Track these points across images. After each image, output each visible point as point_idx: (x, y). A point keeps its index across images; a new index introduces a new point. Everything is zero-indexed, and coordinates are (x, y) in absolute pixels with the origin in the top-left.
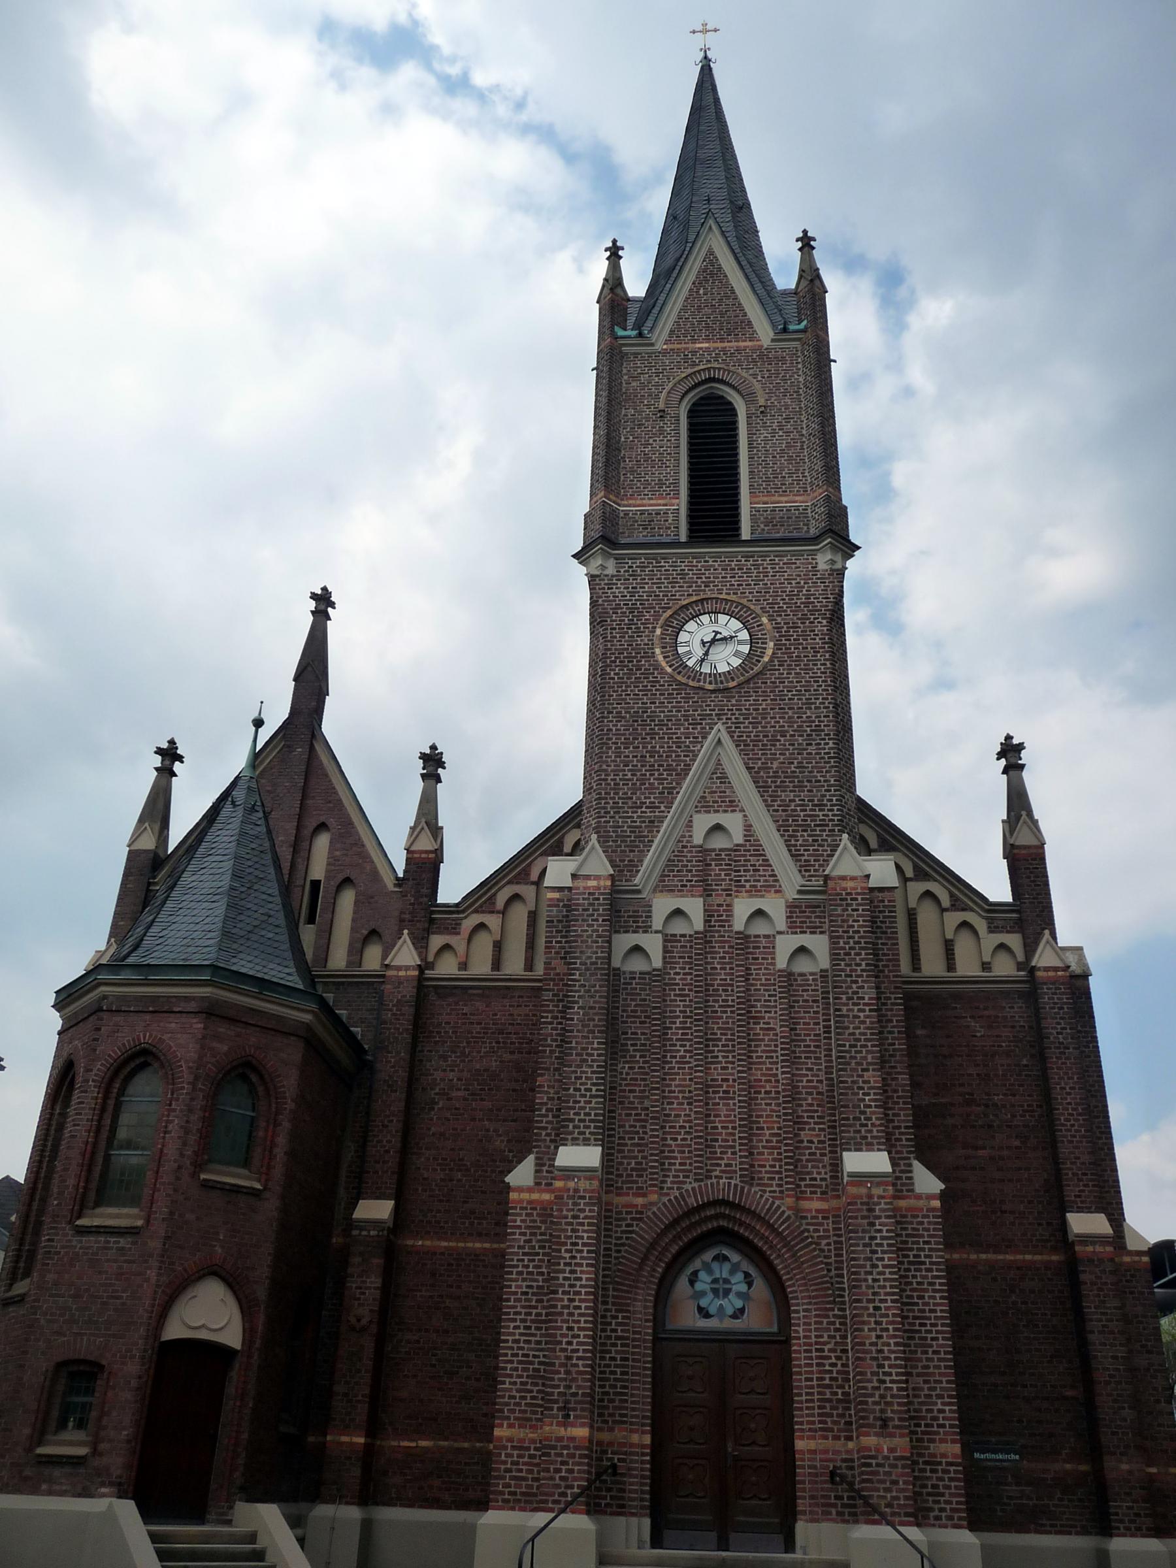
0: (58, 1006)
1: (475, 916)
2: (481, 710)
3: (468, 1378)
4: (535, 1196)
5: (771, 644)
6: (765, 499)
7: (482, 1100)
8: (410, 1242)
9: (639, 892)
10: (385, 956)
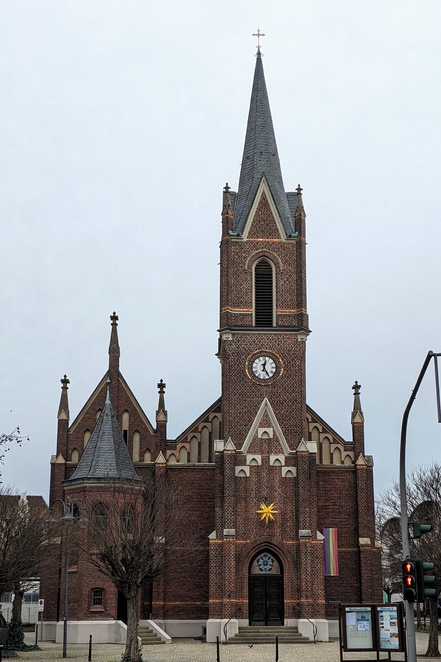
1: (180, 444)
4: (217, 541)
5: (282, 369)
6: (282, 310)
9: (242, 453)
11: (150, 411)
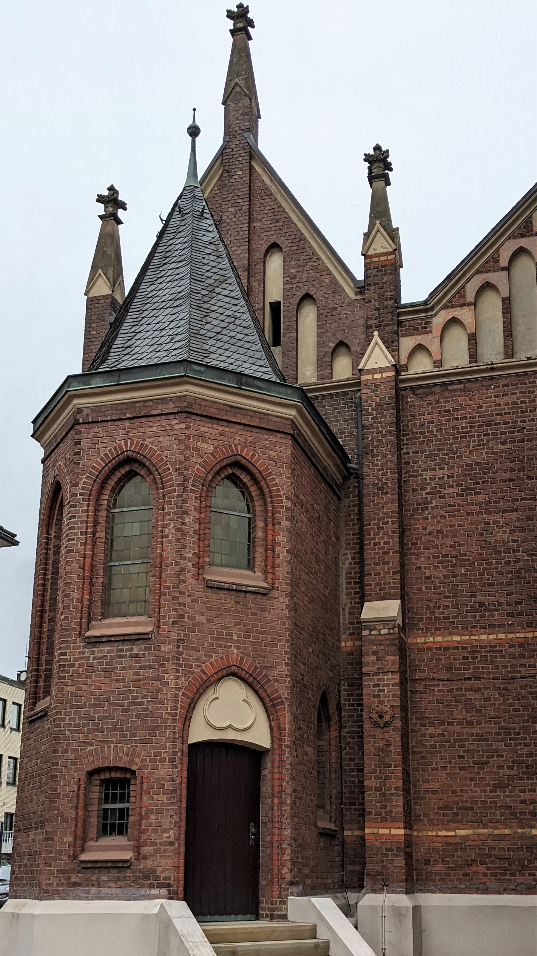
0: (37, 435)
1: (443, 312)
3: (501, 767)
7: (477, 494)
10: (356, 362)
11: (346, 235)
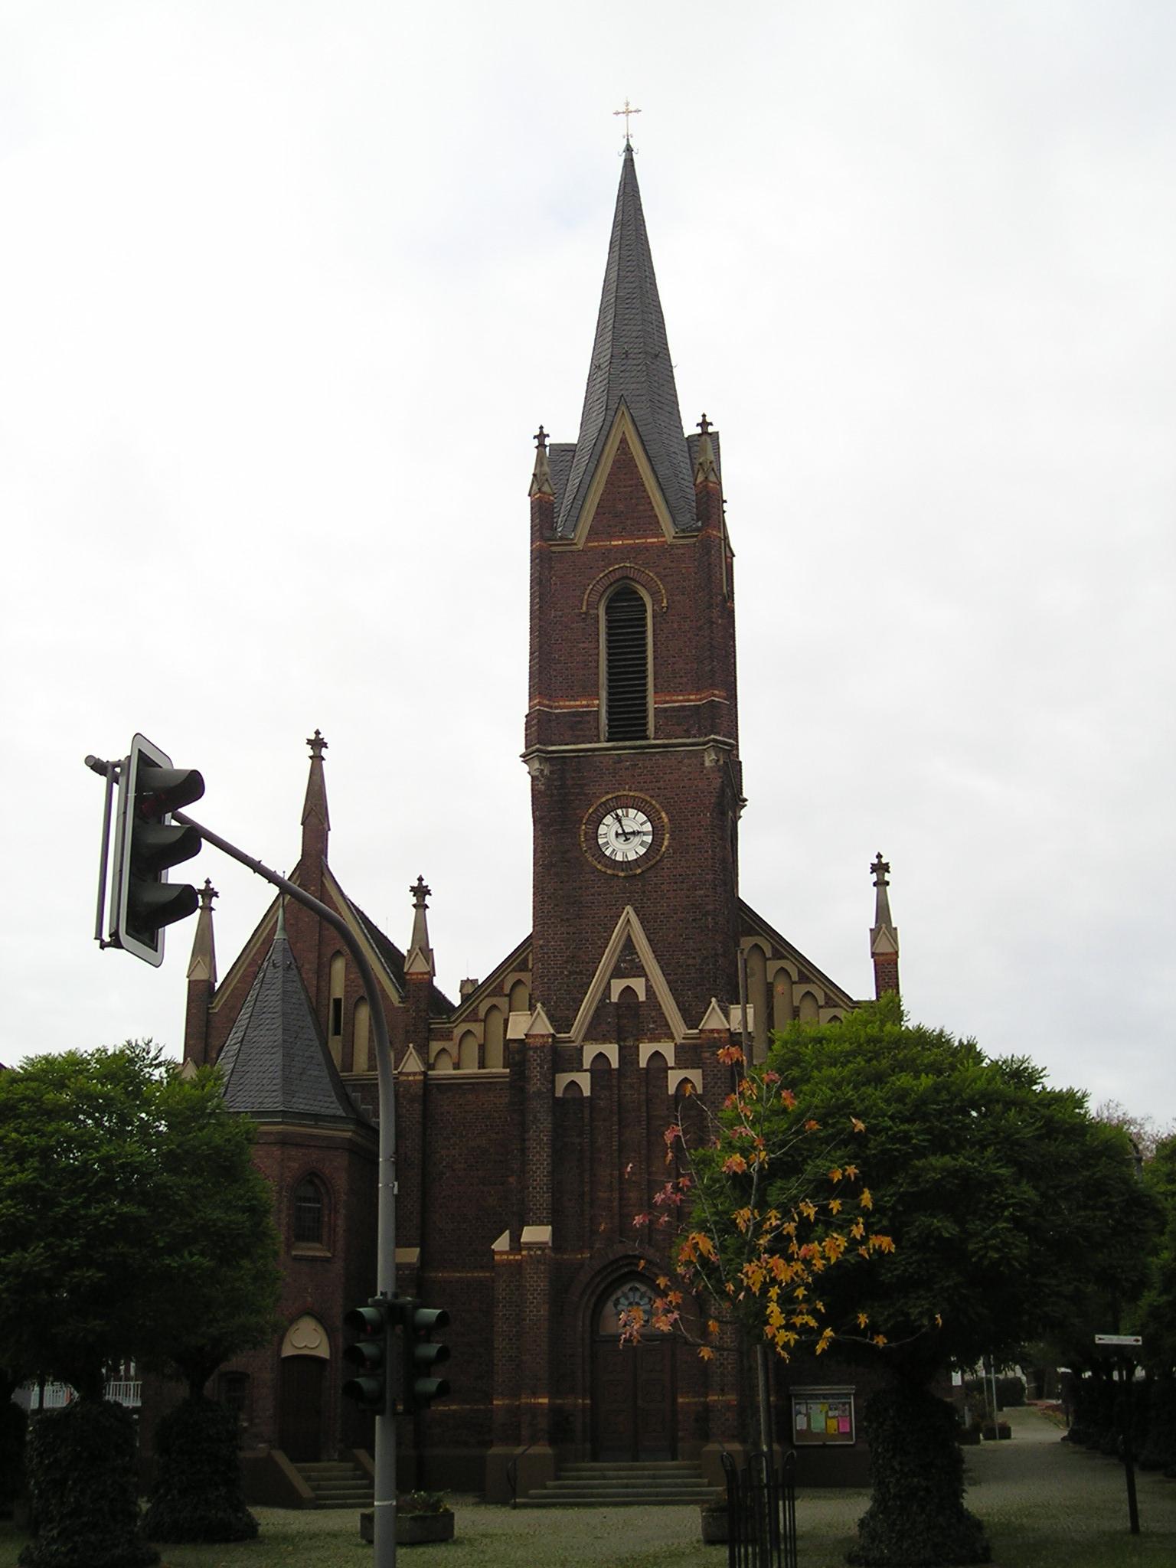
2: (457, 876)
8: (433, 1275)
